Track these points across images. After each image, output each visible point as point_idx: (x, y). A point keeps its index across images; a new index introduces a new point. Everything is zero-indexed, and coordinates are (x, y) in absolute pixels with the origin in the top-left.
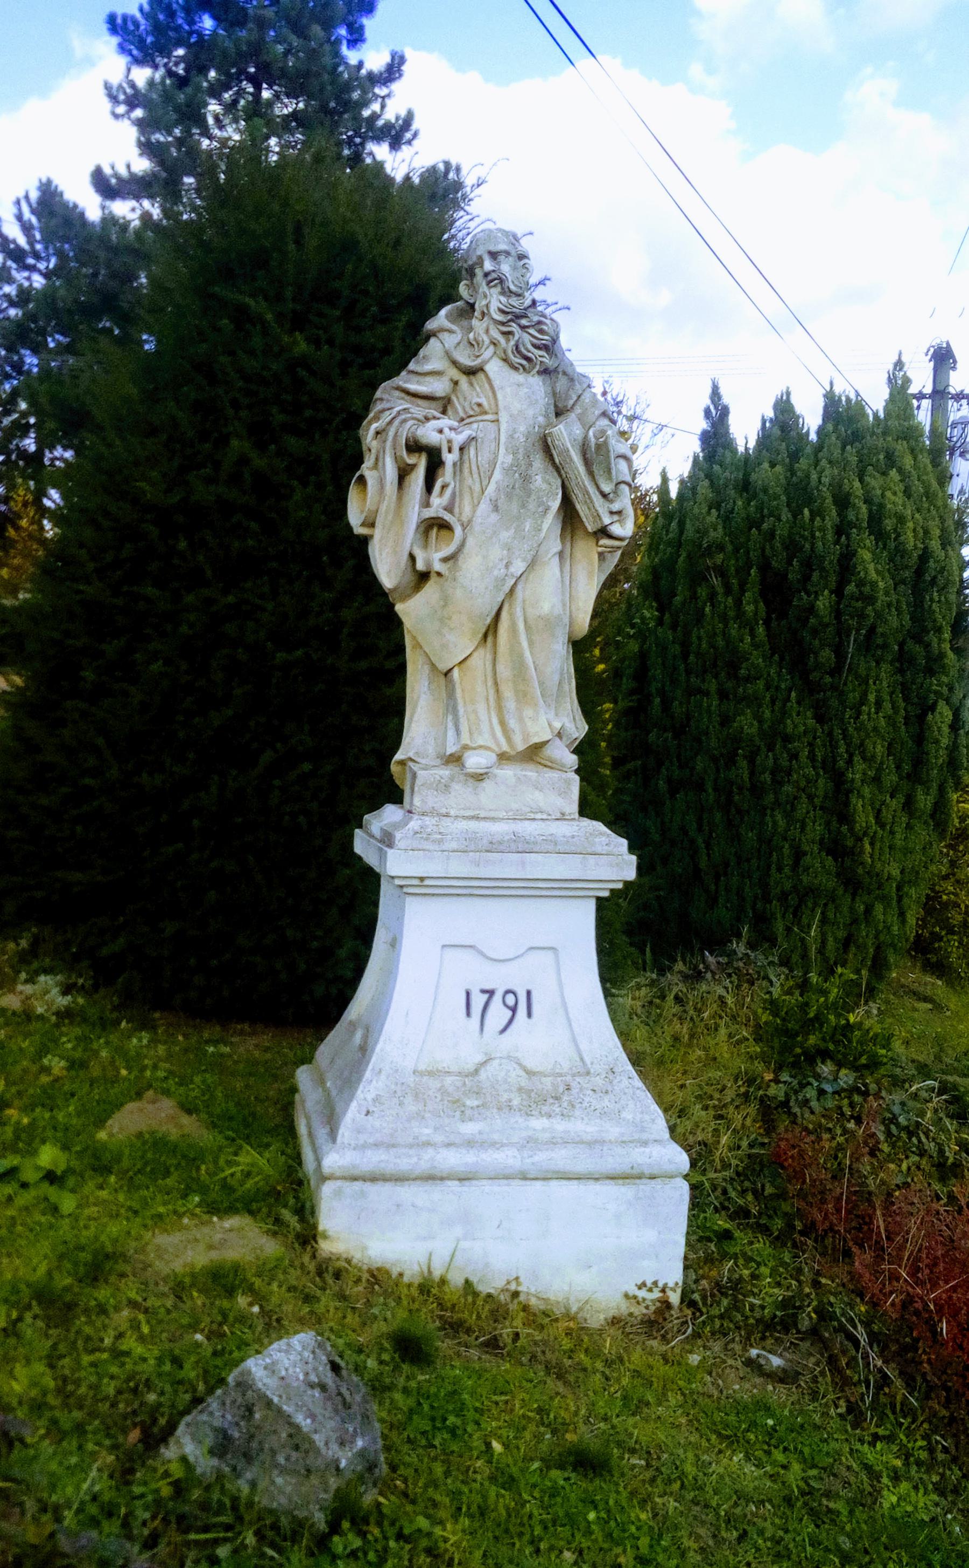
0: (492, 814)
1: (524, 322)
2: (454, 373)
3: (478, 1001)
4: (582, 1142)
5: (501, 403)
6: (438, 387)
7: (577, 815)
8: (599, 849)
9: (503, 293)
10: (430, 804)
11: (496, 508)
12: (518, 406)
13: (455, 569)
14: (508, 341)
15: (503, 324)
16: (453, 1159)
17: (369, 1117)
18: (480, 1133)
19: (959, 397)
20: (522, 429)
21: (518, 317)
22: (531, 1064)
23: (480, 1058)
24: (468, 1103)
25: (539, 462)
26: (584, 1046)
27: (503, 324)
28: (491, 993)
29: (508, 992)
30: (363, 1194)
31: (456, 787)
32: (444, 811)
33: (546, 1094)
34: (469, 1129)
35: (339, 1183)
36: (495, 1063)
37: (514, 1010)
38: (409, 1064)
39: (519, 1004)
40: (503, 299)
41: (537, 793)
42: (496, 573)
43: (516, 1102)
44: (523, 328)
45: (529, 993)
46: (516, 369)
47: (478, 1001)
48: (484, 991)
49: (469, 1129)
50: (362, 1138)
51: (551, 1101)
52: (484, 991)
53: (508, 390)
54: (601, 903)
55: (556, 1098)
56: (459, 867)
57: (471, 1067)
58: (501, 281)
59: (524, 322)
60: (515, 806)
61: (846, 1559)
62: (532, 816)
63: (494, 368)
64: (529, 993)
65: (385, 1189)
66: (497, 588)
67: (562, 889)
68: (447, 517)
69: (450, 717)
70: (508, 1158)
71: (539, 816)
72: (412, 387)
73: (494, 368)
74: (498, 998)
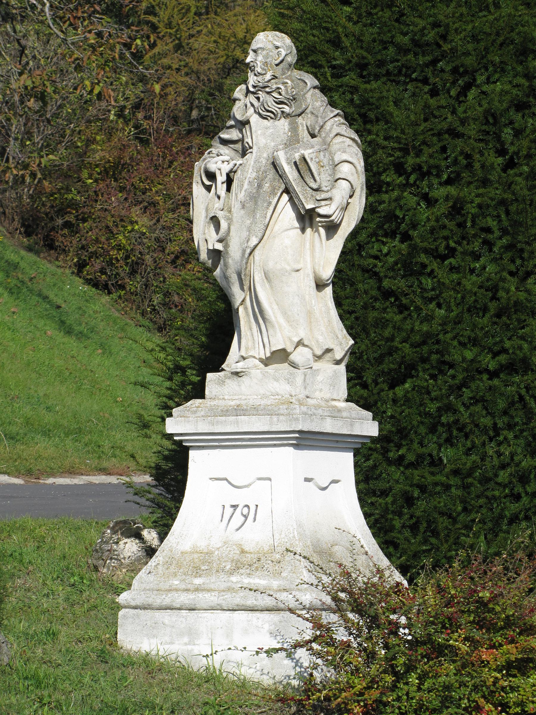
1: (267, 90)
8: (282, 412)
10: (214, 393)
12: (264, 141)
16: (183, 599)
19: (2, 82)
20: (265, 155)
25: (272, 173)
26: (277, 537)
28: (235, 507)
30: (138, 616)
32: (221, 397)
34: (198, 581)
35: (127, 610)
37: (246, 517)
40: (255, 78)
41: (275, 383)
44: (268, 93)
47: (229, 511)
48: (233, 506)
49: (198, 581)
50: (144, 586)
51: (246, 566)
55: (250, 566)
59: (267, 90)
60: (262, 392)
63: (254, 119)
65: (149, 613)
70: (211, 598)
73: (254, 119)
74: (239, 510)
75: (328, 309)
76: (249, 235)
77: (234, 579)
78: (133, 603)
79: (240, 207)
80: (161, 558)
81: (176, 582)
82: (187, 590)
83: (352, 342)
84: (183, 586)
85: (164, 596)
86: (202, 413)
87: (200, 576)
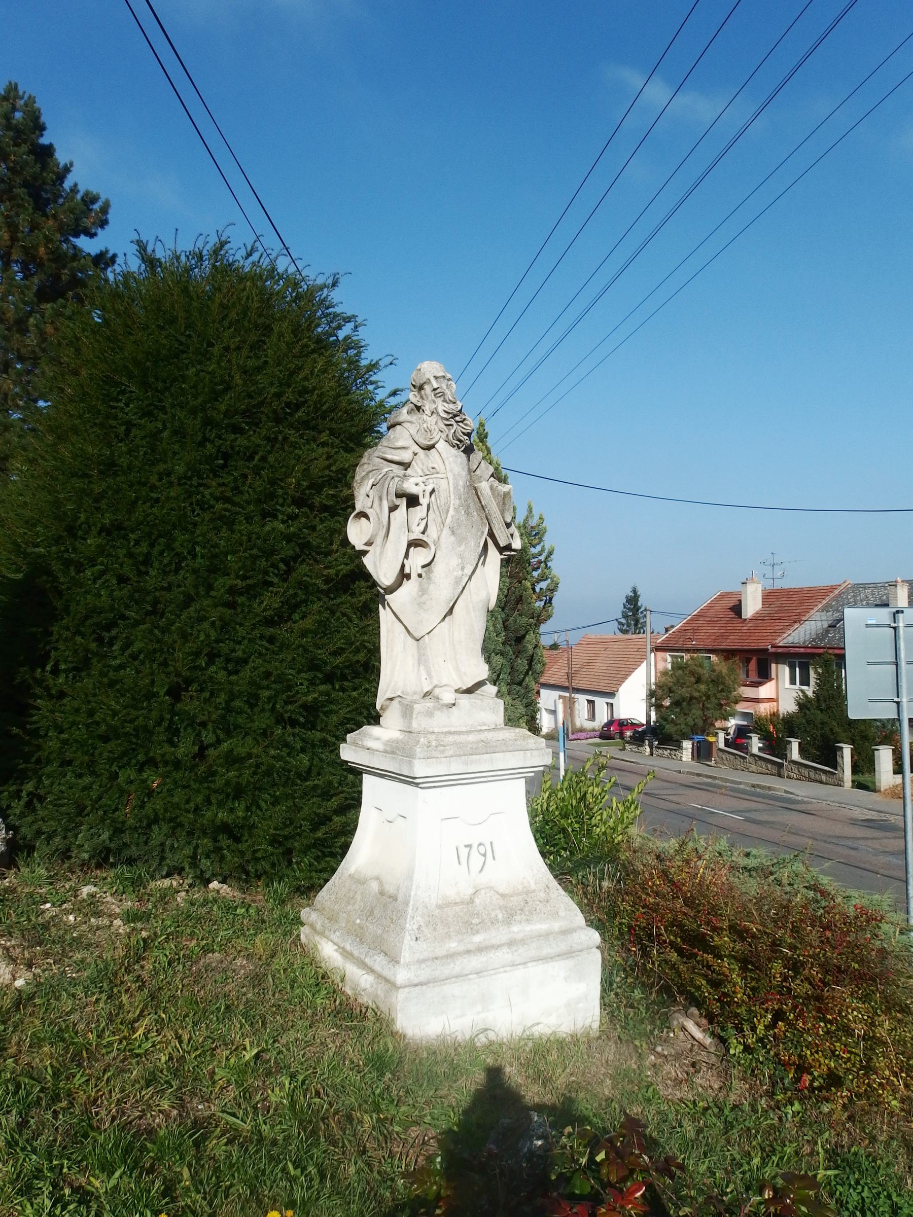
0: (458, 729)
2: (416, 449)
3: (464, 852)
4: (540, 936)
5: (448, 468)
6: (406, 456)
7: (503, 725)
8: (530, 746)
9: (445, 401)
11: (453, 533)
13: (430, 571)
14: (449, 430)
15: (447, 420)
17: (419, 942)
18: (484, 940)
20: (461, 483)
21: (456, 416)
22: (501, 891)
23: (471, 891)
24: (474, 922)
27: (447, 420)
28: (469, 846)
29: (480, 844)
31: (437, 713)
32: (431, 730)
33: (516, 906)
35: (407, 990)
36: (483, 892)
37: (484, 855)
38: (434, 902)
39: (488, 852)
42: (455, 573)
43: (500, 916)
45: (491, 843)
46: (454, 447)
47: (464, 852)
48: (466, 846)
49: (478, 939)
52: (466, 846)
53: (451, 459)
54: (529, 782)
56: (456, 767)
57: (467, 897)
58: (444, 394)
61: (2, 1190)
62: (479, 728)
63: (442, 446)
64: (491, 843)
66: (457, 583)
67: (509, 774)
68: (424, 538)
69: (422, 667)
71: (483, 728)
72: (389, 457)
73: (442, 446)
75: (388, 631)
76: (462, 563)
77: (515, 928)
78: (416, 981)
79: (450, 533)
80: (419, 918)
81: (454, 945)
82: (468, 952)
83: (853, 715)
84: (462, 948)
85: (452, 965)
86: (451, 752)
87: (478, 932)
